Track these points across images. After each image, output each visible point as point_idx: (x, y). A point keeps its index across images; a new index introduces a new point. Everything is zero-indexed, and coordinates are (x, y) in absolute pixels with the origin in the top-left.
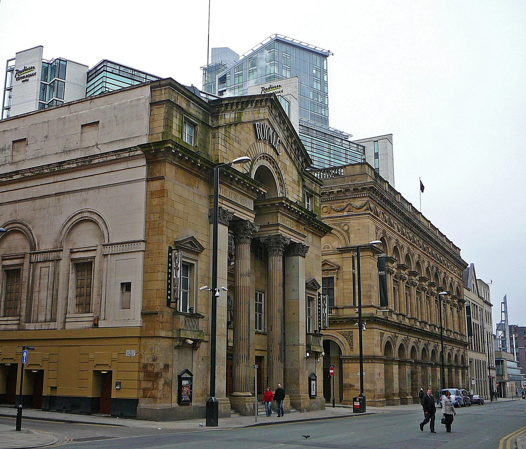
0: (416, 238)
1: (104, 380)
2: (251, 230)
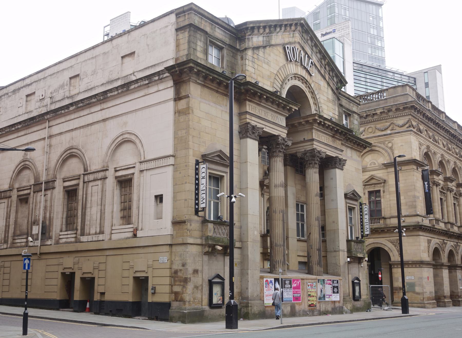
0: (422, 127)
1: (141, 283)
2: (283, 144)
